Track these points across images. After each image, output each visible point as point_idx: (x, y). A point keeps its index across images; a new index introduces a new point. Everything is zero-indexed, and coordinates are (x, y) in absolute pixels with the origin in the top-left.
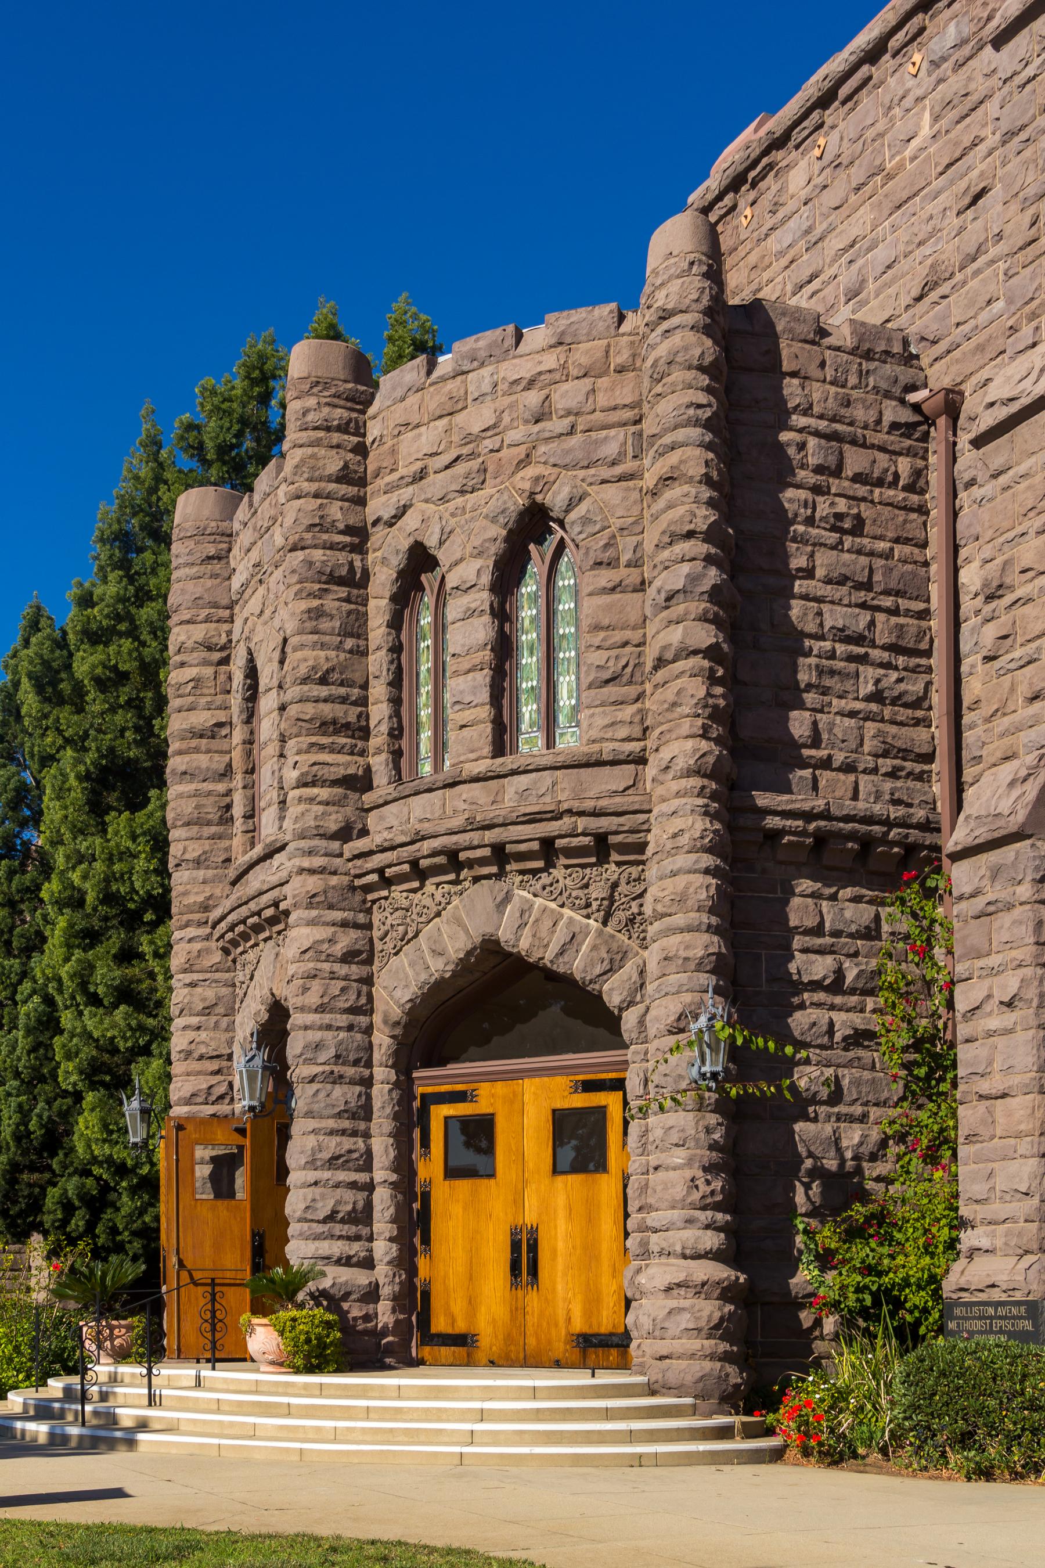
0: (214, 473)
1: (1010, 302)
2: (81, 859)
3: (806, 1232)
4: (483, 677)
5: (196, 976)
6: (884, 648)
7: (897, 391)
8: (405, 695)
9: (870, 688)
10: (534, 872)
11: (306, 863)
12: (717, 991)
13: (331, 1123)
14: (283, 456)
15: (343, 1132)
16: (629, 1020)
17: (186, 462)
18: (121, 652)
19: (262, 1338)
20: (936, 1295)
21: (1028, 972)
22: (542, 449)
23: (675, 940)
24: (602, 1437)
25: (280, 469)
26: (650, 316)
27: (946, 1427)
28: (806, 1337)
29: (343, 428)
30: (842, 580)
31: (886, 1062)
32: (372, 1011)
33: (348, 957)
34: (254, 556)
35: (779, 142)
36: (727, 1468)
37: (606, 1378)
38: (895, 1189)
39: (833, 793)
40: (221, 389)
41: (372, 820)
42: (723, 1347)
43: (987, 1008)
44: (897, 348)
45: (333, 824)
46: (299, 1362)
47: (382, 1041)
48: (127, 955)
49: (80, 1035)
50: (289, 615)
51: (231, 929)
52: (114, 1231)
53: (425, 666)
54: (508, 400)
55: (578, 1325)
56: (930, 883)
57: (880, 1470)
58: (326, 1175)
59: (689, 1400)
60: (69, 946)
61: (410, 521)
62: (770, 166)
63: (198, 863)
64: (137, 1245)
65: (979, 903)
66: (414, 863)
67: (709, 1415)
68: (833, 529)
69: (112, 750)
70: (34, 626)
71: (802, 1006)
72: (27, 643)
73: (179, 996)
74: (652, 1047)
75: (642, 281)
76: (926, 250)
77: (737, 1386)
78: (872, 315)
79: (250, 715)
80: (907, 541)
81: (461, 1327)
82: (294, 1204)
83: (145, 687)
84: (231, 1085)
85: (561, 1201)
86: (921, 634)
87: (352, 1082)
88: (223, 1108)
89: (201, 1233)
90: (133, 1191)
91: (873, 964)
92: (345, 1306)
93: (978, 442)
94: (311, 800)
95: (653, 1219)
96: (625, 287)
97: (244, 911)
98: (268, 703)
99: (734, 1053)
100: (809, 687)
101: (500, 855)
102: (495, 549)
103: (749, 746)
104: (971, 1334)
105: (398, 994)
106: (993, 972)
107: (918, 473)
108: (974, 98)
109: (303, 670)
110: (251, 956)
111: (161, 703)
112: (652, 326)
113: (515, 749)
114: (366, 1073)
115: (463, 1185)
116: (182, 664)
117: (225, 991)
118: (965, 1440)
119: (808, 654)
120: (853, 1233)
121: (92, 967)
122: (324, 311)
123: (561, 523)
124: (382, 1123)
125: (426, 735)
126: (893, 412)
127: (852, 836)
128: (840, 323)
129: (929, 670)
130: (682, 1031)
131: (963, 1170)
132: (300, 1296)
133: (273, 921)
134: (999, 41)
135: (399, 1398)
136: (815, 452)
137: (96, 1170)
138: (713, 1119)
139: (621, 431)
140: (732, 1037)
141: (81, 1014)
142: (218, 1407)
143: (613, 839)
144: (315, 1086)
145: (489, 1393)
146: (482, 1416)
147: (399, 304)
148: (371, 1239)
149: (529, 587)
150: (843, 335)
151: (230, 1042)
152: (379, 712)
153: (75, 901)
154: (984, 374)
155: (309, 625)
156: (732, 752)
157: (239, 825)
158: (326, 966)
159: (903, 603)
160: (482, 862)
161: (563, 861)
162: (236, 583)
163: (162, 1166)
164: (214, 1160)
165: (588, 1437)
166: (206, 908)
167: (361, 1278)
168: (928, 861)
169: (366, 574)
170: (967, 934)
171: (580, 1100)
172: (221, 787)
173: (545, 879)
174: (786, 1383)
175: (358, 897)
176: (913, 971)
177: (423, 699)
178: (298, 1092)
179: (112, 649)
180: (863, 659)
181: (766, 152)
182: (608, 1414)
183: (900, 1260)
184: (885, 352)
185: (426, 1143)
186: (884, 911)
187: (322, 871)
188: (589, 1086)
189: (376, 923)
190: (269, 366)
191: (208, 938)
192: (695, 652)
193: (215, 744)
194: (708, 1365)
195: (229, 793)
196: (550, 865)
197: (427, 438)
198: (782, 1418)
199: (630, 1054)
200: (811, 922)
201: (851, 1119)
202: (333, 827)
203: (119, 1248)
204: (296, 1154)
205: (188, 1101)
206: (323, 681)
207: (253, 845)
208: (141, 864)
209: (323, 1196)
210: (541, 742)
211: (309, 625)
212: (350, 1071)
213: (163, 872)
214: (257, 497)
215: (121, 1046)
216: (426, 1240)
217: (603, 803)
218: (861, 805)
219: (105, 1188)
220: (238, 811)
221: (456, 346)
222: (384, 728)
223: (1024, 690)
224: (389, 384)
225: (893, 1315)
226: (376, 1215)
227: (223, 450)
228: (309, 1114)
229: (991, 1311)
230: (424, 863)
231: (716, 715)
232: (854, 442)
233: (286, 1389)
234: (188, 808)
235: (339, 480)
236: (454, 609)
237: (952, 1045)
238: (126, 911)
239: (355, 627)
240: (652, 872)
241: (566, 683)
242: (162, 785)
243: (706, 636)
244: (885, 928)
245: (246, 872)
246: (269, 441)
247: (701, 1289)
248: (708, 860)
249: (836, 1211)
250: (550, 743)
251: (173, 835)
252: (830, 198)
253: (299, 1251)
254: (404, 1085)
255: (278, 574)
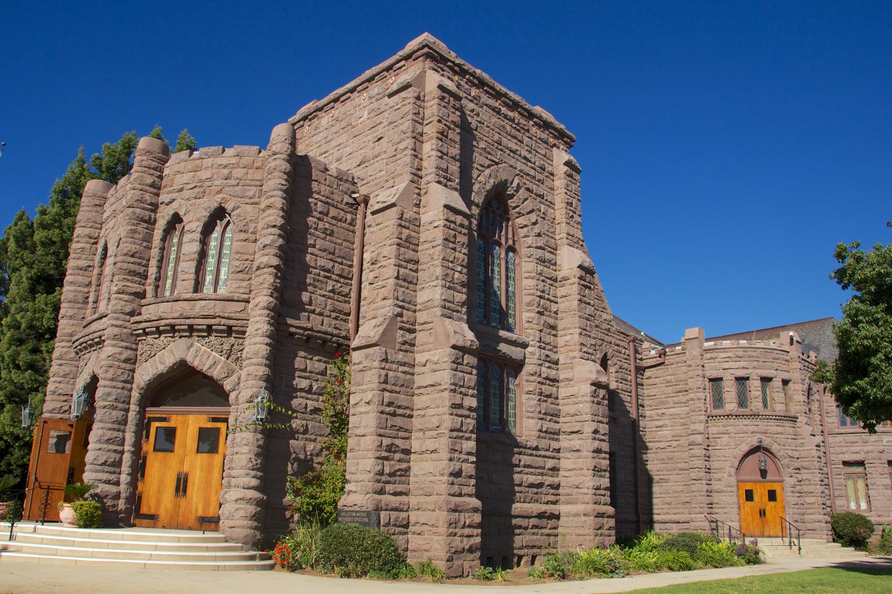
0: (104, 176)
1: (387, 172)
2: (22, 310)
3: (290, 481)
4: (193, 264)
5: (62, 362)
6: (337, 275)
7: (349, 192)
8: (163, 266)
9: (331, 288)
10: (203, 337)
11: (115, 323)
12: (266, 388)
13: (110, 426)
14: (130, 174)
15: (114, 429)
16: (232, 396)
17: (94, 169)
18: (54, 234)
19: (67, 512)
20: (336, 508)
21: (375, 392)
22: (226, 189)
23: (253, 368)
24: (204, 558)
25: (129, 178)
26: (270, 153)
27: (335, 557)
28: (288, 521)
29: (155, 169)
30: (325, 250)
31: (325, 420)
32: (133, 383)
33: (126, 361)
34: (114, 207)
35: (320, 109)
36: (252, 572)
37: (209, 535)
38: (324, 467)
39: (315, 322)
40: (112, 147)
41: (143, 310)
42: (255, 524)
43: (361, 404)
44: (350, 179)
45: (128, 309)
46: (82, 523)
47: (135, 395)
48: (35, 351)
49: (9, 381)
50: (123, 230)
51: (80, 345)
52: (9, 464)
53: (173, 256)
54: (216, 171)
55: (200, 513)
56: (345, 358)
57: (309, 573)
58: (105, 446)
59: (240, 545)
60: (10, 344)
61: (175, 205)
62: (316, 116)
63: (71, 317)
64: (18, 471)
65: (361, 367)
66: (158, 328)
67: (247, 551)
68: (323, 233)
69: (43, 270)
70: (21, 219)
71: (296, 397)
72: (16, 224)
73: (54, 369)
74: (240, 407)
75: (268, 141)
76: (362, 151)
77: (259, 540)
78: (344, 168)
79: (102, 265)
80: (348, 241)
81: (153, 511)
82: (89, 457)
83: (62, 248)
84: (70, 407)
85: (199, 463)
86: (350, 272)
87: (121, 410)
88: (66, 416)
89: (46, 465)
90: (21, 447)
91: (323, 384)
92: (105, 500)
93: (373, 213)
94: (121, 299)
95: (234, 473)
96: (263, 142)
97: (87, 338)
98: (109, 261)
99: (270, 412)
100: (310, 284)
101: (191, 329)
102: (204, 220)
103: (287, 300)
104: (346, 523)
105: (144, 377)
106: (364, 391)
107: (353, 220)
108: (382, 110)
109: (125, 251)
110: (87, 356)
111: (67, 255)
112: (270, 156)
113: (202, 291)
114: (127, 406)
115: (161, 455)
116: (78, 242)
117: (74, 369)
118: (341, 562)
119: (311, 273)
120: (308, 483)
121: (19, 354)
122: (157, 129)
123: (230, 215)
124: (131, 427)
125: (169, 281)
126: (347, 199)
127: (320, 338)
128: (333, 168)
129: (351, 285)
130: (251, 402)
131: (348, 462)
132: (86, 495)
133: (98, 343)
134: (390, 96)
135: (122, 540)
136: (320, 207)
137: (5, 438)
138: (260, 436)
139: (255, 188)
140: (270, 406)
141: (10, 372)
142: (42, 541)
143: (234, 328)
144: (105, 410)
145: (160, 539)
146: (156, 548)
147: (184, 131)
148: (120, 473)
149: (216, 235)
150: (333, 171)
151: (73, 389)
152: (152, 271)
153: (17, 326)
154: (377, 193)
155: (130, 235)
156: (280, 303)
157: (91, 305)
158: (117, 363)
159: (345, 261)
160: (184, 331)
161: (214, 334)
162: (105, 216)
163: (35, 438)
164: (58, 437)
165: (199, 558)
166: (71, 335)
167: (113, 489)
168: (345, 350)
169: (155, 221)
170: (356, 377)
171: (210, 425)
172: (86, 290)
173: (207, 340)
174: (278, 539)
175: (134, 338)
176: (336, 388)
177: (170, 268)
178: (97, 412)
179: (50, 232)
180: (329, 278)
181: (315, 111)
182: (208, 549)
183: (323, 494)
184: (346, 180)
185: (148, 436)
186: (329, 366)
187: (121, 326)
188: (215, 420)
189: (139, 349)
190: (132, 143)
191: (70, 347)
192: (271, 266)
193: (86, 273)
194: (249, 531)
195: (88, 292)
196: (209, 335)
197: (186, 178)
198: (275, 553)
199: (231, 409)
200: (302, 367)
201: (310, 440)
202: (128, 310)
203: (10, 472)
204: (93, 437)
205: (51, 412)
206: (132, 256)
207: (95, 313)
208: (47, 315)
209: (102, 455)
210: (212, 290)
211: (130, 235)
212: (121, 405)
213: (56, 320)
214: (118, 187)
215: (26, 387)
216: (143, 476)
217: (231, 315)
218: (324, 328)
219: (8, 446)
220: (91, 300)
221: (201, 149)
222: (153, 277)
223: (381, 296)
224: (174, 157)
225: (319, 514)
226: (123, 464)
227: (109, 168)
228: (101, 421)
230: (161, 328)
231: (276, 289)
232: (333, 206)
233: (74, 534)
234: (71, 296)
235: (150, 186)
236: (186, 238)
237: (348, 416)
238: (38, 333)
239: (148, 238)
240: (247, 342)
241: (224, 270)
242: (62, 286)
243: (276, 261)
244: (328, 372)
245: (90, 323)
246: (127, 169)
247: (249, 501)
248: (267, 340)
249: (302, 474)
250: (215, 291)
251: (62, 305)
252: (334, 129)
253: (88, 476)
254: (142, 413)
255: (122, 215)
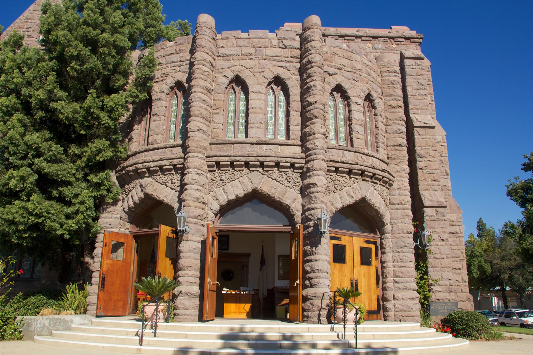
85: (362, 273)
171: (366, 245)
229: (444, 304)
